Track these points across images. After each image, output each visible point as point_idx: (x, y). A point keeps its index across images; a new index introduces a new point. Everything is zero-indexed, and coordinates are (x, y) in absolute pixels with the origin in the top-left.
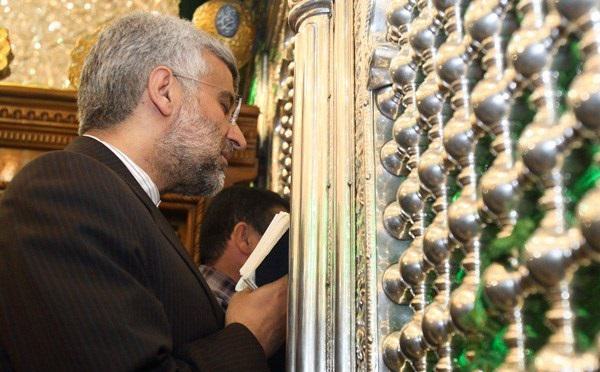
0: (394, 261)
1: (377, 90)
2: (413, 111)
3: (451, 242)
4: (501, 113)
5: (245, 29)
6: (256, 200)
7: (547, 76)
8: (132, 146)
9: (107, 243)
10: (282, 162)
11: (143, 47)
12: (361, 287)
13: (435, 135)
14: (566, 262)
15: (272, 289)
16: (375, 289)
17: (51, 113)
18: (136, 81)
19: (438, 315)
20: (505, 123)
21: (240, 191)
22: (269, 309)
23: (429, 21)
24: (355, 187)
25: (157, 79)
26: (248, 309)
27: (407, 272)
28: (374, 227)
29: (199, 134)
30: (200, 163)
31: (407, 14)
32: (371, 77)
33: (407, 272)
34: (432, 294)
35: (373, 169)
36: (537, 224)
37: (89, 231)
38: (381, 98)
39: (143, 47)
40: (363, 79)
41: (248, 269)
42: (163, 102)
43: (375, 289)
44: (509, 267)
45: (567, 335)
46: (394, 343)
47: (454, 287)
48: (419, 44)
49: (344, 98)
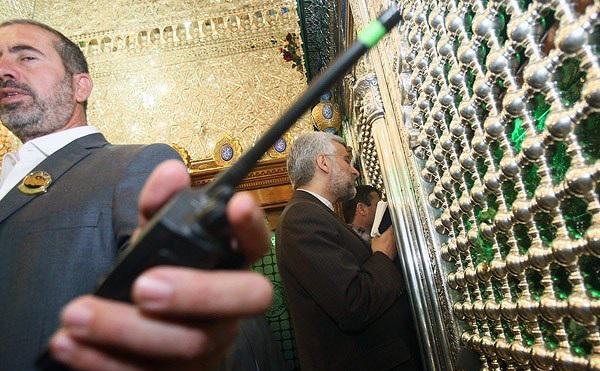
0: (423, 167)
1: (414, 149)
2: (423, 95)
3: (462, 170)
4: (472, 113)
5: (336, 113)
6: (369, 194)
7: (491, 96)
8: (317, 189)
9: (325, 234)
10: (367, 169)
11: (310, 148)
12: (426, 229)
13: (435, 100)
14: (509, 223)
15: (387, 233)
16: (432, 230)
17: (265, 171)
18: (312, 163)
19: (463, 240)
20: (475, 116)
21: (362, 194)
22: (390, 239)
23: (430, 82)
24: (414, 189)
25: (320, 160)
26: (380, 245)
27: (430, 170)
28: (426, 204)
29: (342, 175)
30: (346, 187)
31: (413, 55)
32: (410, 144)
33: (430, 170)
34: (450, 202)
35: (420, 180)
36: (497, 210)
37: (318, 232)
38: (416, 151)
39: (310, 148)
40: (406, 145)
41: (375, 229)
42: (325, 168)
43: (432, 230)
44: (488, 223)
45: (516, 248)
46: (445, 250)
47: (459, 197)
48: (421, 66)
49: (400, 154)
